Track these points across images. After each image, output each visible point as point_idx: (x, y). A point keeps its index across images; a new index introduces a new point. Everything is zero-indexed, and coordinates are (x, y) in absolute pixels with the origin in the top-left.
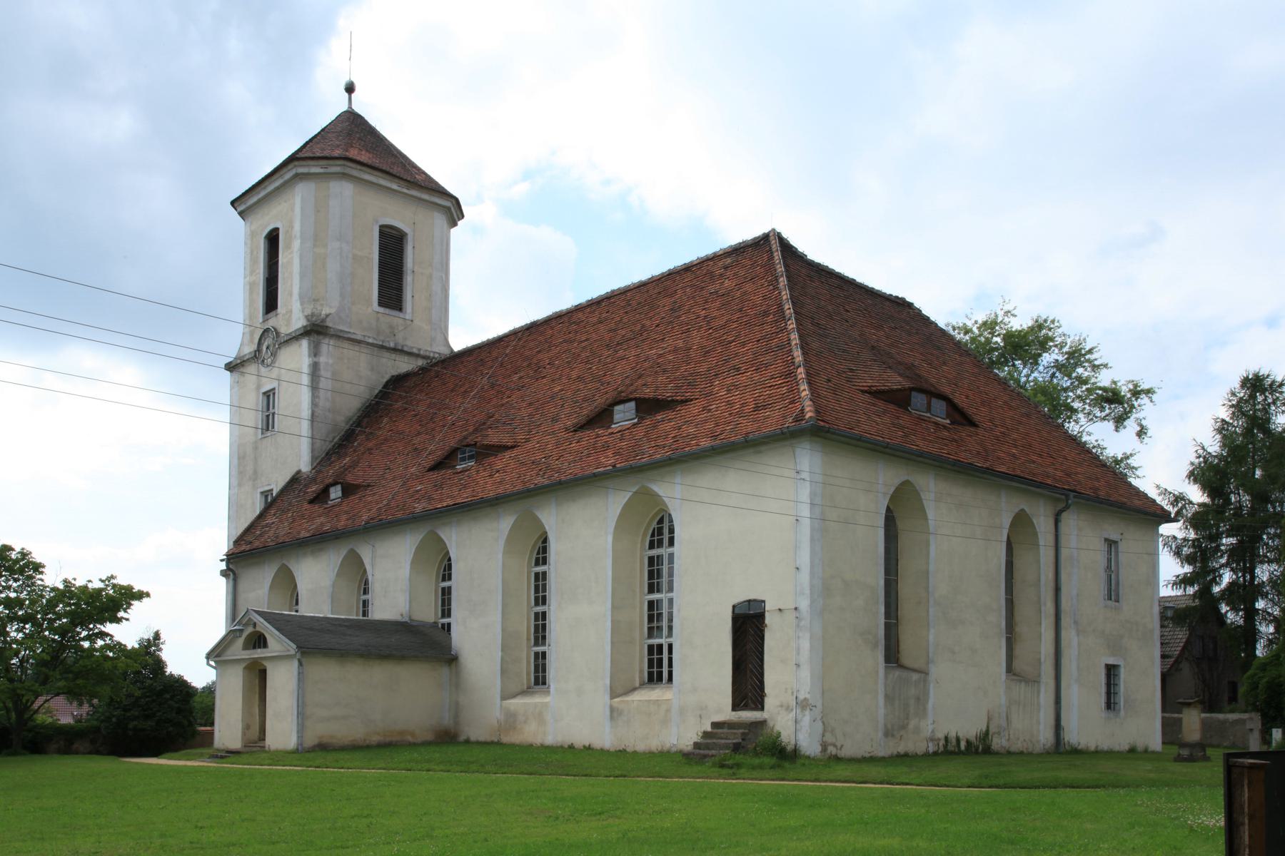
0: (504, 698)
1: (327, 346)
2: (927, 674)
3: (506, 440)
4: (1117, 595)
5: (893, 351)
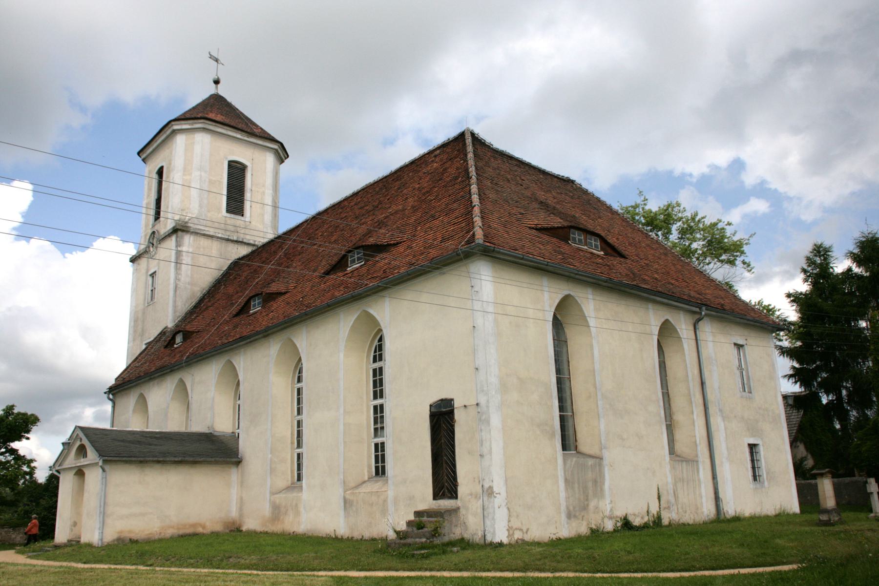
0: (273, 493)
1: (188, 239)
2: (601, 459)
3: (282, 289)
4: (750, 388)
5: (558, 206)
